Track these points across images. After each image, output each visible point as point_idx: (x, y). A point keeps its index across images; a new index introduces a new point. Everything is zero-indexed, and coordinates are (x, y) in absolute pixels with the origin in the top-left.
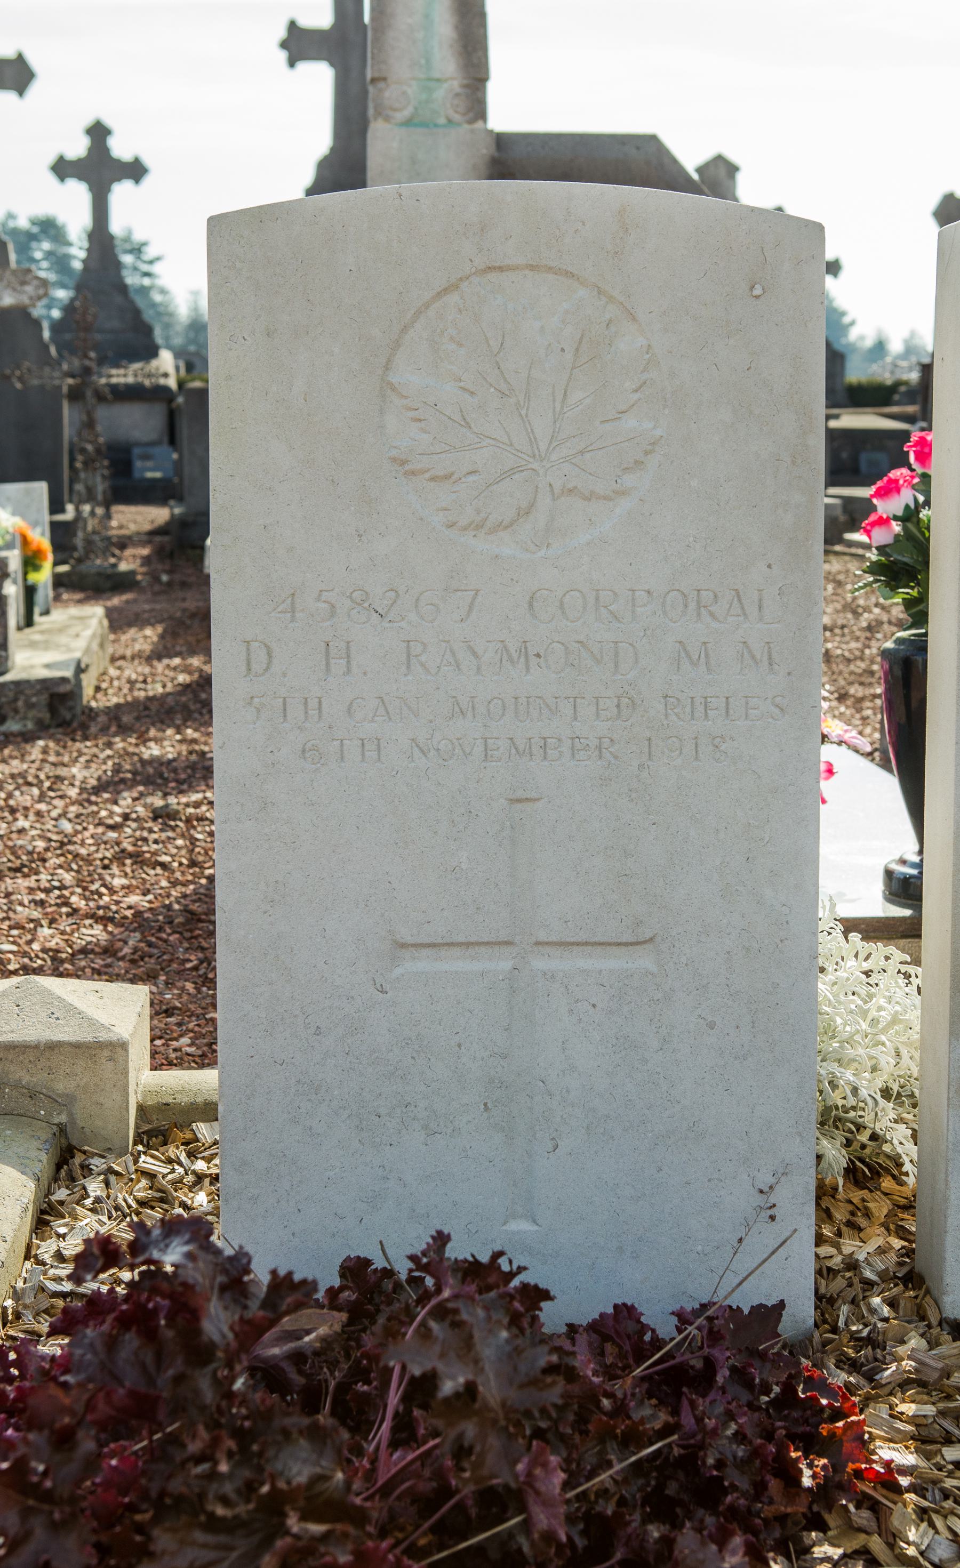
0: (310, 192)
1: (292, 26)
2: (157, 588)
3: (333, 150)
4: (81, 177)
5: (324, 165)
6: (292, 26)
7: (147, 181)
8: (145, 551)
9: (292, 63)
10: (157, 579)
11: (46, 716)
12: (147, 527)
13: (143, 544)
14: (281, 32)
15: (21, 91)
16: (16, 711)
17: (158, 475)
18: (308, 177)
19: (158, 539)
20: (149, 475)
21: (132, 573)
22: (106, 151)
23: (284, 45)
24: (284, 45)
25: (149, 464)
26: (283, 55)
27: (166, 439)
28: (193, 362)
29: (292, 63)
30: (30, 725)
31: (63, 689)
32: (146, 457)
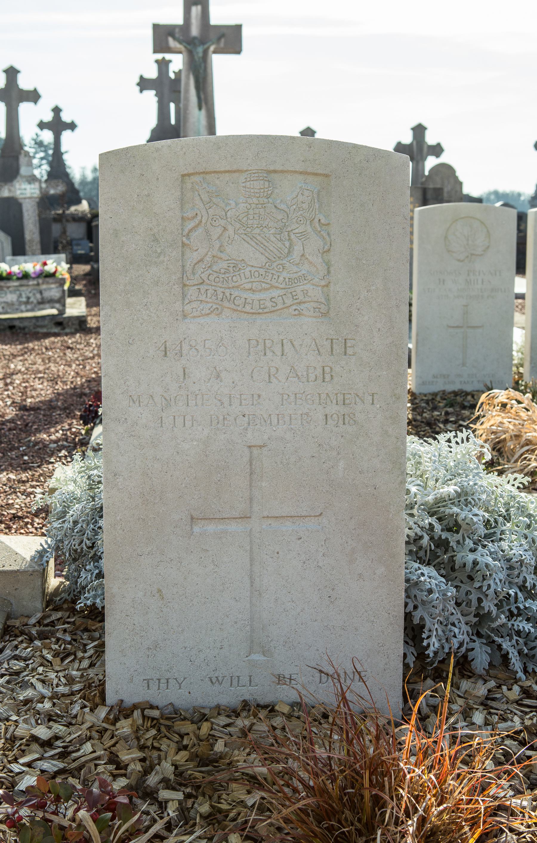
0: (148, 142)
1: (141, 77)
2: (90, 295)
3: (157, 125)
4: (50, 129)
5: (153, 131)
6: (141, 77)
7: (77, 130)
8: (84, 282)
9: (141, 91)
10: (90, 292)
11: (78, 327)
12: (82, 273)
13: (83, 280)
14: (137, 80)
15: (35, 102)
16: (68, 326)
17: (82, 252)
18: (148, 136)
19: (88, 277)
20: (80, 252)
21: (80, 290)
22: (60, 118)
23: (138, 84)
24: (138, 84)
25: (79, 247)
26: (138, 88)
27: (86, 237)
28: (93, 204)
29: (141, 91)
30: (73, 330)
31: (83, 319)
32: (78, 245)
